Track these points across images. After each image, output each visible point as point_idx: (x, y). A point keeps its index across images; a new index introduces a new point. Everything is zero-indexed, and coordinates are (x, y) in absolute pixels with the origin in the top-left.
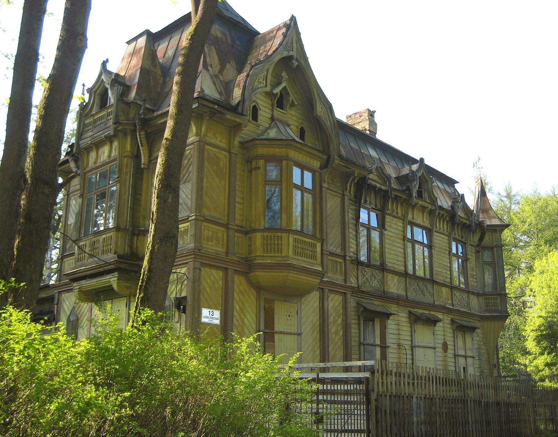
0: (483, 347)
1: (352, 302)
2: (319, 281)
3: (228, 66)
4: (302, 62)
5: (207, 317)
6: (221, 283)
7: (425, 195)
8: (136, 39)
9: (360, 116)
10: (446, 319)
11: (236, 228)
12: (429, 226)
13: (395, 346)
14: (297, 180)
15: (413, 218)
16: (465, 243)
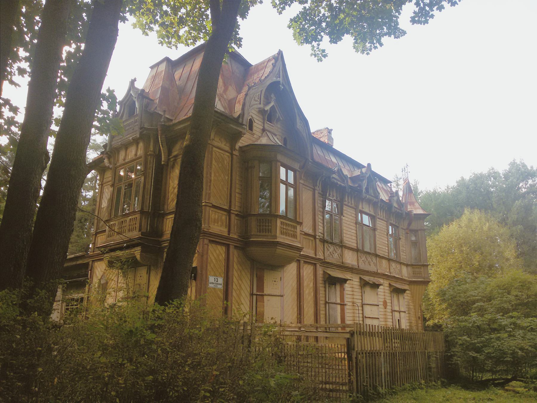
0: (411, 304)
1: (320, 271)
2: (298, 255)
3: (230, 88)
4: (287, 87)
5: (213, 283)
6: (224, 256)
7: (371, 191)
8: (158, 65)
9: (321, 133)
10: (386, 283)
11: (236, 213)
12: (373, 214)
13: (350, 304)
14: (283, 177)
15: (363, 208)
16: (398, 227)
